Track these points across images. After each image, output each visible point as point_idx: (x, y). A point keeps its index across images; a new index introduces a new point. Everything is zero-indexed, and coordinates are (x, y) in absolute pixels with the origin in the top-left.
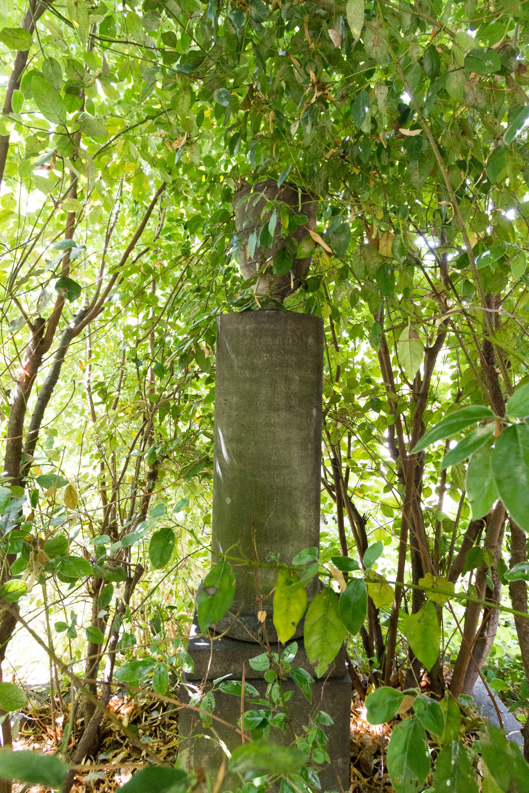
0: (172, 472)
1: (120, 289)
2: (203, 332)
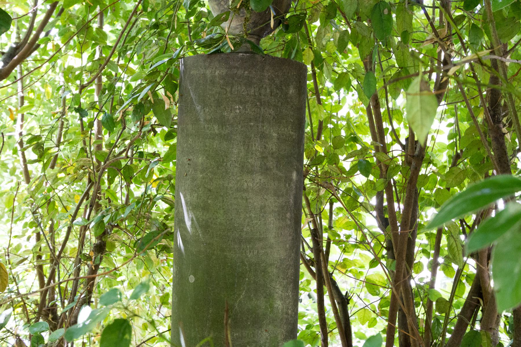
0: (123, 243)
1: (59, 23)
2: (162, 78)
